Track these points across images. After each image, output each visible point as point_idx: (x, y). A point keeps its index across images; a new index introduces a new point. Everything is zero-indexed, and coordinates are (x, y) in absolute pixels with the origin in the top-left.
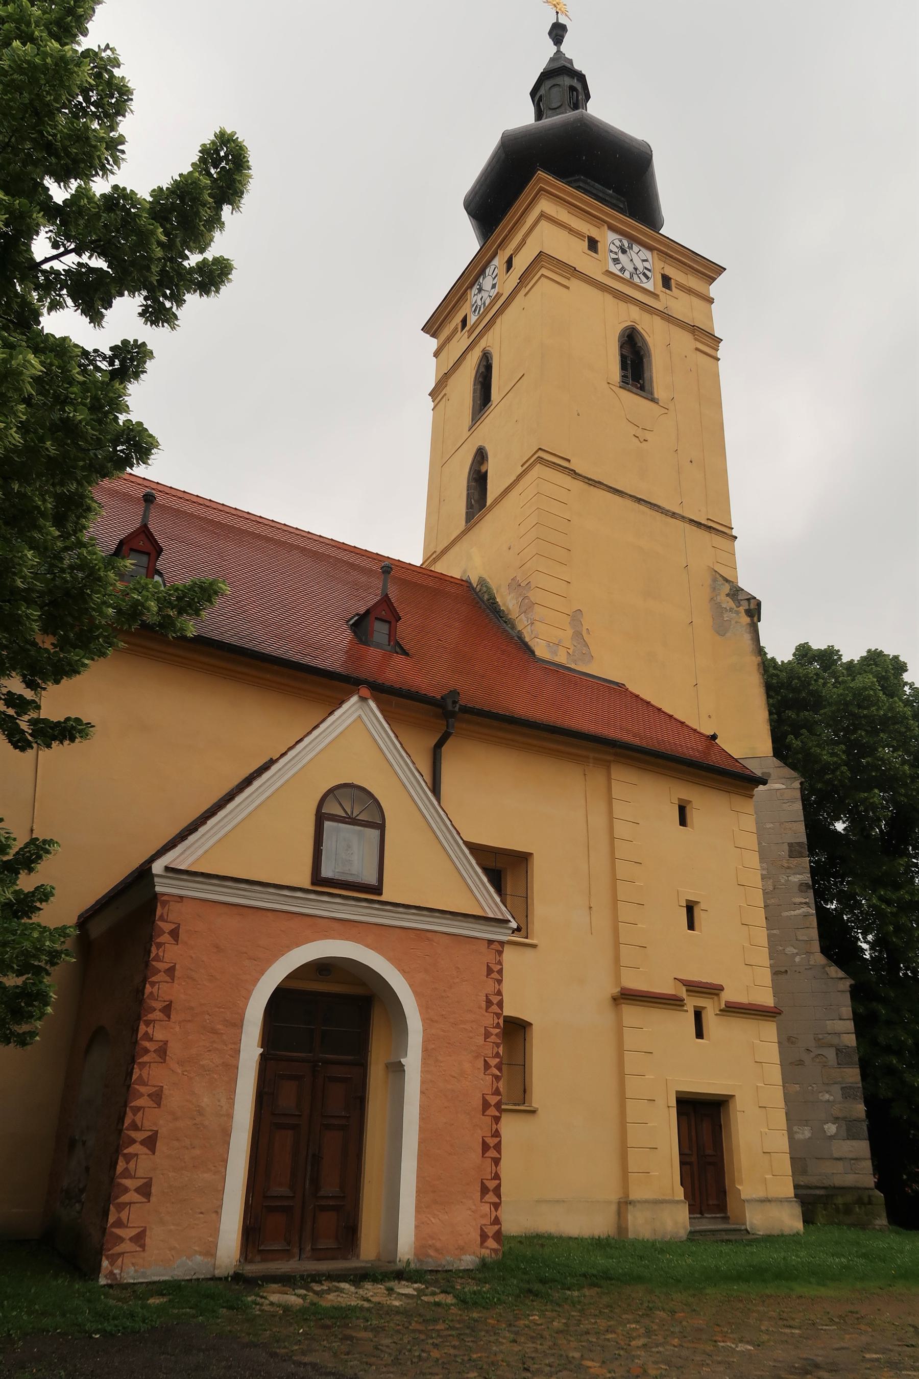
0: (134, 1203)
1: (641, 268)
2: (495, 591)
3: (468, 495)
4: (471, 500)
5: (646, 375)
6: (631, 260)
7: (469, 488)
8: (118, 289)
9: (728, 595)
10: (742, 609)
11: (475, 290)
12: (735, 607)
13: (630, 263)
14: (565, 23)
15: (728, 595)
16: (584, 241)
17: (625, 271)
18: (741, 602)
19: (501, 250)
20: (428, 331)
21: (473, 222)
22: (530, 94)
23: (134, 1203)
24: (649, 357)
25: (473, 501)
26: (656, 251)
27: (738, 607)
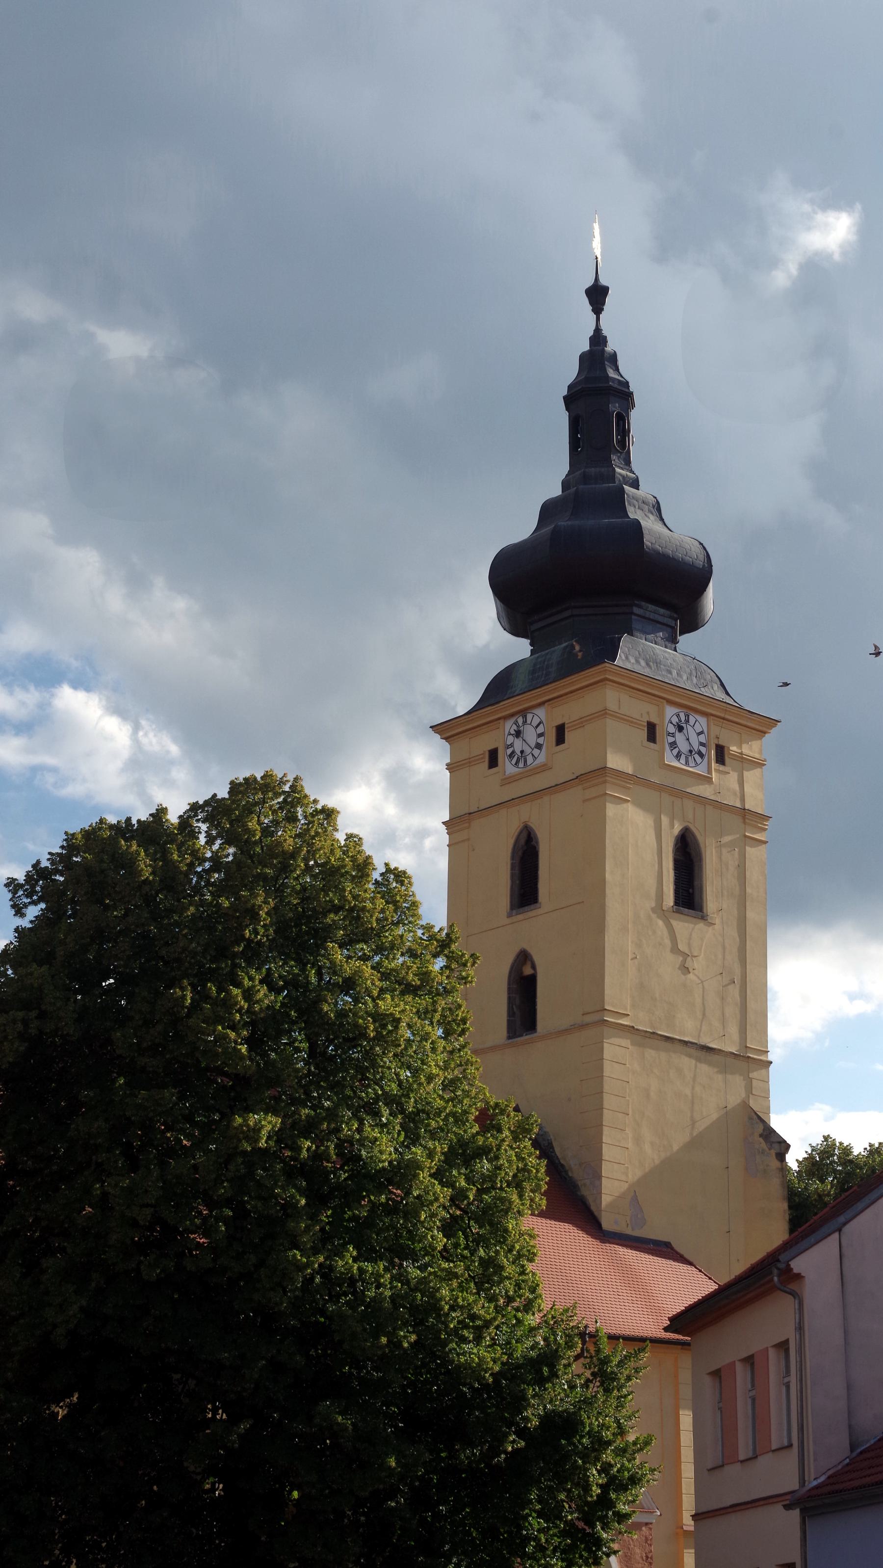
0: (720, 1382)
1: (696, 746)
2: (552, 1137)
3: (509, 998)
4: (512, 1006)
5: (696, 883)
6: (688, 739)
7: (510, 990)
8: (214, 832)
9: (761, 1136)
10: (773, 1152)
11: (510, 726)
12: (767, 1149)
13: (686, 743)
14: (649, 743)
15: (761, 1136)
16: (644, 730)
17: (676, 747)
18: (773, 1145)
19: (548, 705)
20: (453, 768)
21: (499, 605)
22: (569, 387)
23: (720, 1382)
24: (700, 862)
25: (514, 1007)
26: (712, 717)
27: (770, 1149)
